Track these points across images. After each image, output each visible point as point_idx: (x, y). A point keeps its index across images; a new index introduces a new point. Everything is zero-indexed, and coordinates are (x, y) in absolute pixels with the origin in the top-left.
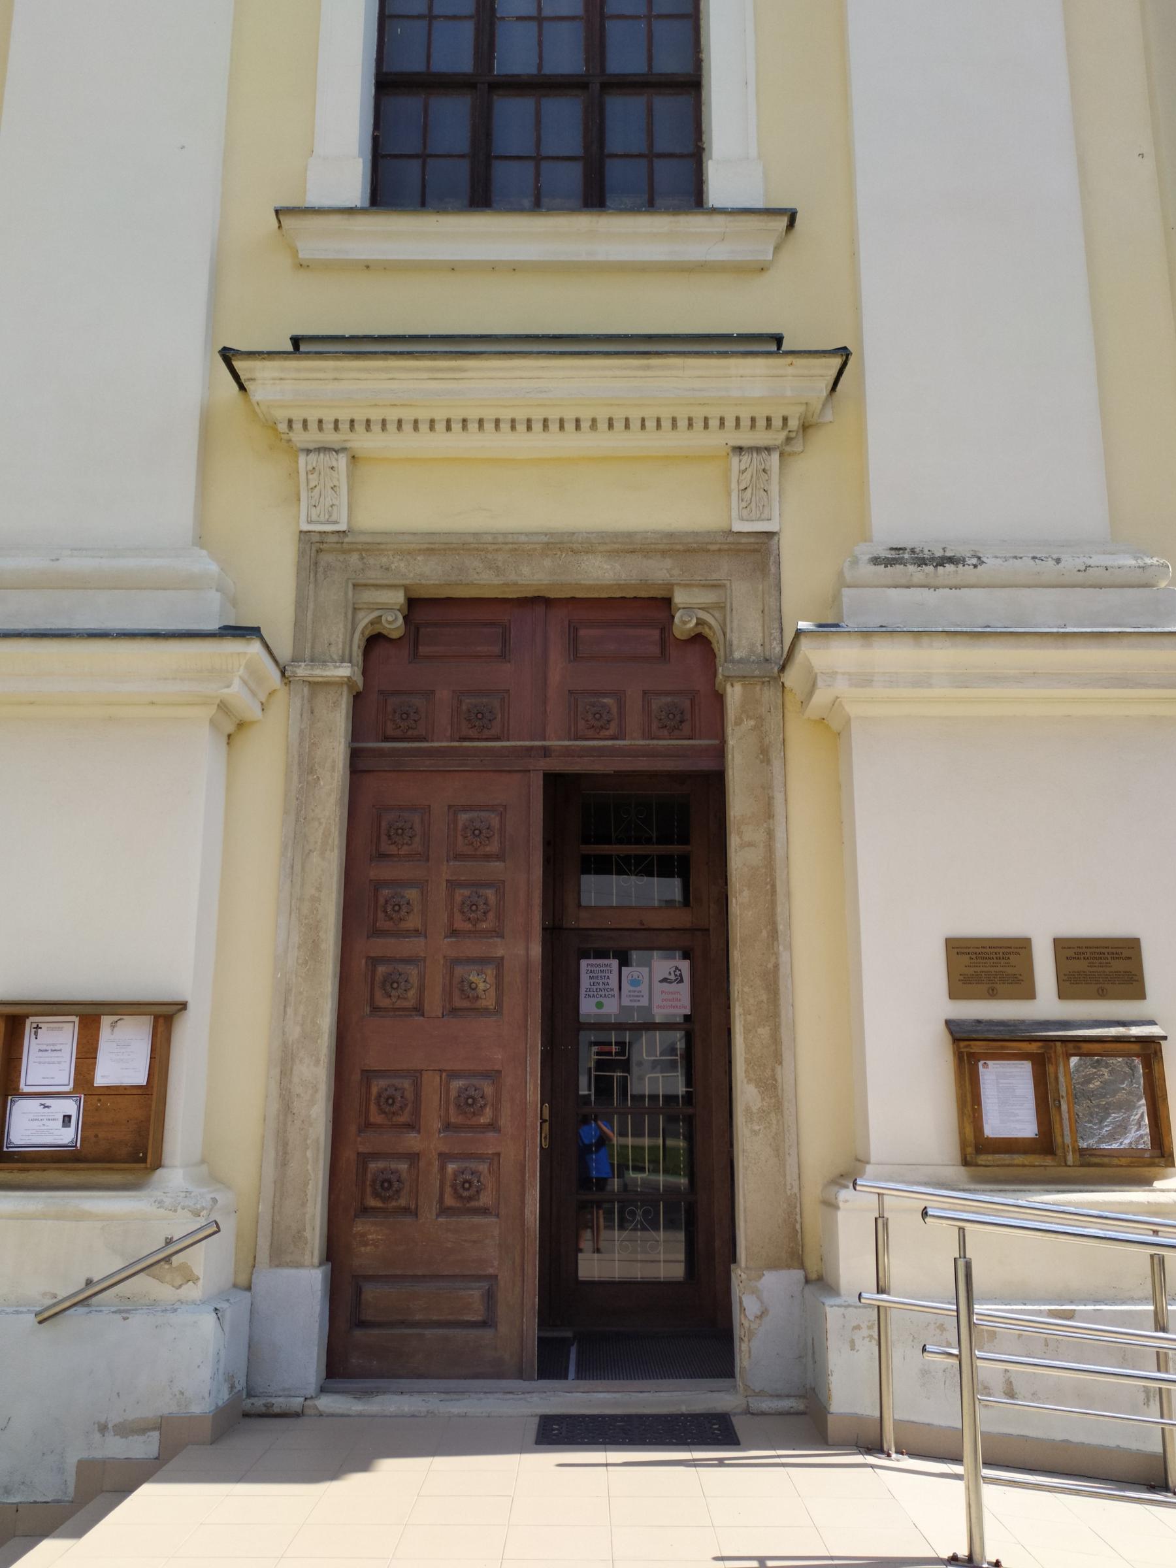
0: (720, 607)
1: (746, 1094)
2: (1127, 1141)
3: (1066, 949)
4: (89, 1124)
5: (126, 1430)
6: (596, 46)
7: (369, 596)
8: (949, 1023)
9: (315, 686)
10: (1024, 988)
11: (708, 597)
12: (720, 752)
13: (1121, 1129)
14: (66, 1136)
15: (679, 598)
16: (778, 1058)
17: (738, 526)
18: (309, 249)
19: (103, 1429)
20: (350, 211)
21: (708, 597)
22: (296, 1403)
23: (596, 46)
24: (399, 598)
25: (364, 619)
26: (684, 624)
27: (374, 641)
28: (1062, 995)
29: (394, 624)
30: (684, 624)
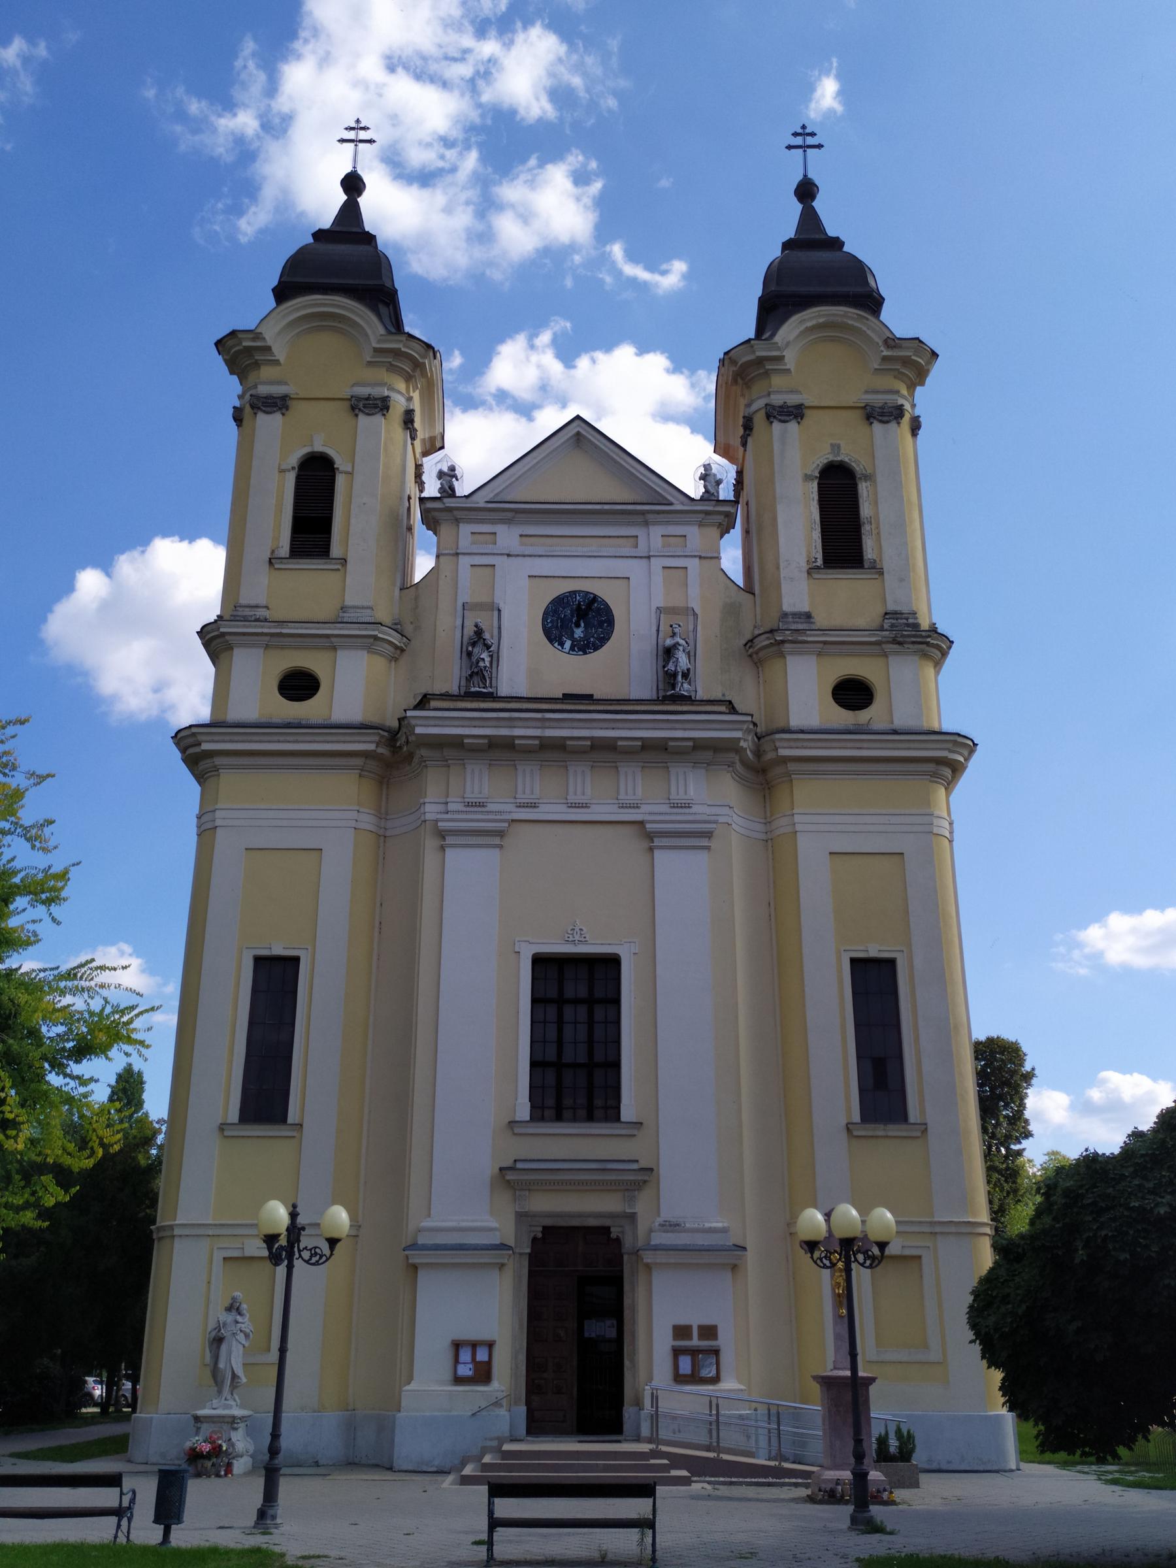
0: (623, 1232)
1: (627, 1363)
2: (140, 1114)
3: (701, 1328)
4: (476, 1370)
5: (491, 1439)
6: (591, 1013)
7: (533, 1228)
8: (673, 1346)
9: (521, 1254)
10: (690, 1337)
11: (620, 1229)
12: (622, 1271)
13: (710, 1372)
14: (470, 1373)
15: (612, 1229)
16: (634, 1354)
17: (627, 1211)
18: (517, 1130)
19: (486, 1439)
20: (275, 308)
21: (620, 1229)
22: (522, 1438)
23: (591, 1013)
24: (541, 1229)
25: (532, 1235)
26: (613, 1235)
27: (534, 1240)
28: (699, 1339)
29: (540, 1235)
30: (613, 1235)
